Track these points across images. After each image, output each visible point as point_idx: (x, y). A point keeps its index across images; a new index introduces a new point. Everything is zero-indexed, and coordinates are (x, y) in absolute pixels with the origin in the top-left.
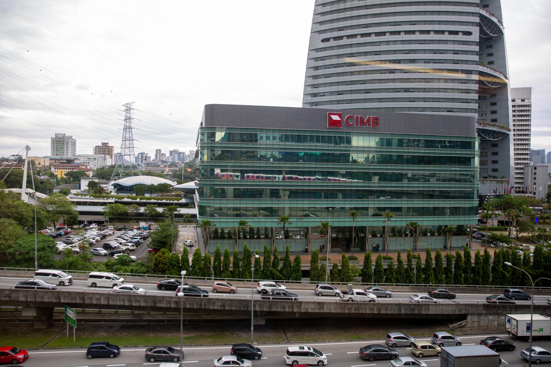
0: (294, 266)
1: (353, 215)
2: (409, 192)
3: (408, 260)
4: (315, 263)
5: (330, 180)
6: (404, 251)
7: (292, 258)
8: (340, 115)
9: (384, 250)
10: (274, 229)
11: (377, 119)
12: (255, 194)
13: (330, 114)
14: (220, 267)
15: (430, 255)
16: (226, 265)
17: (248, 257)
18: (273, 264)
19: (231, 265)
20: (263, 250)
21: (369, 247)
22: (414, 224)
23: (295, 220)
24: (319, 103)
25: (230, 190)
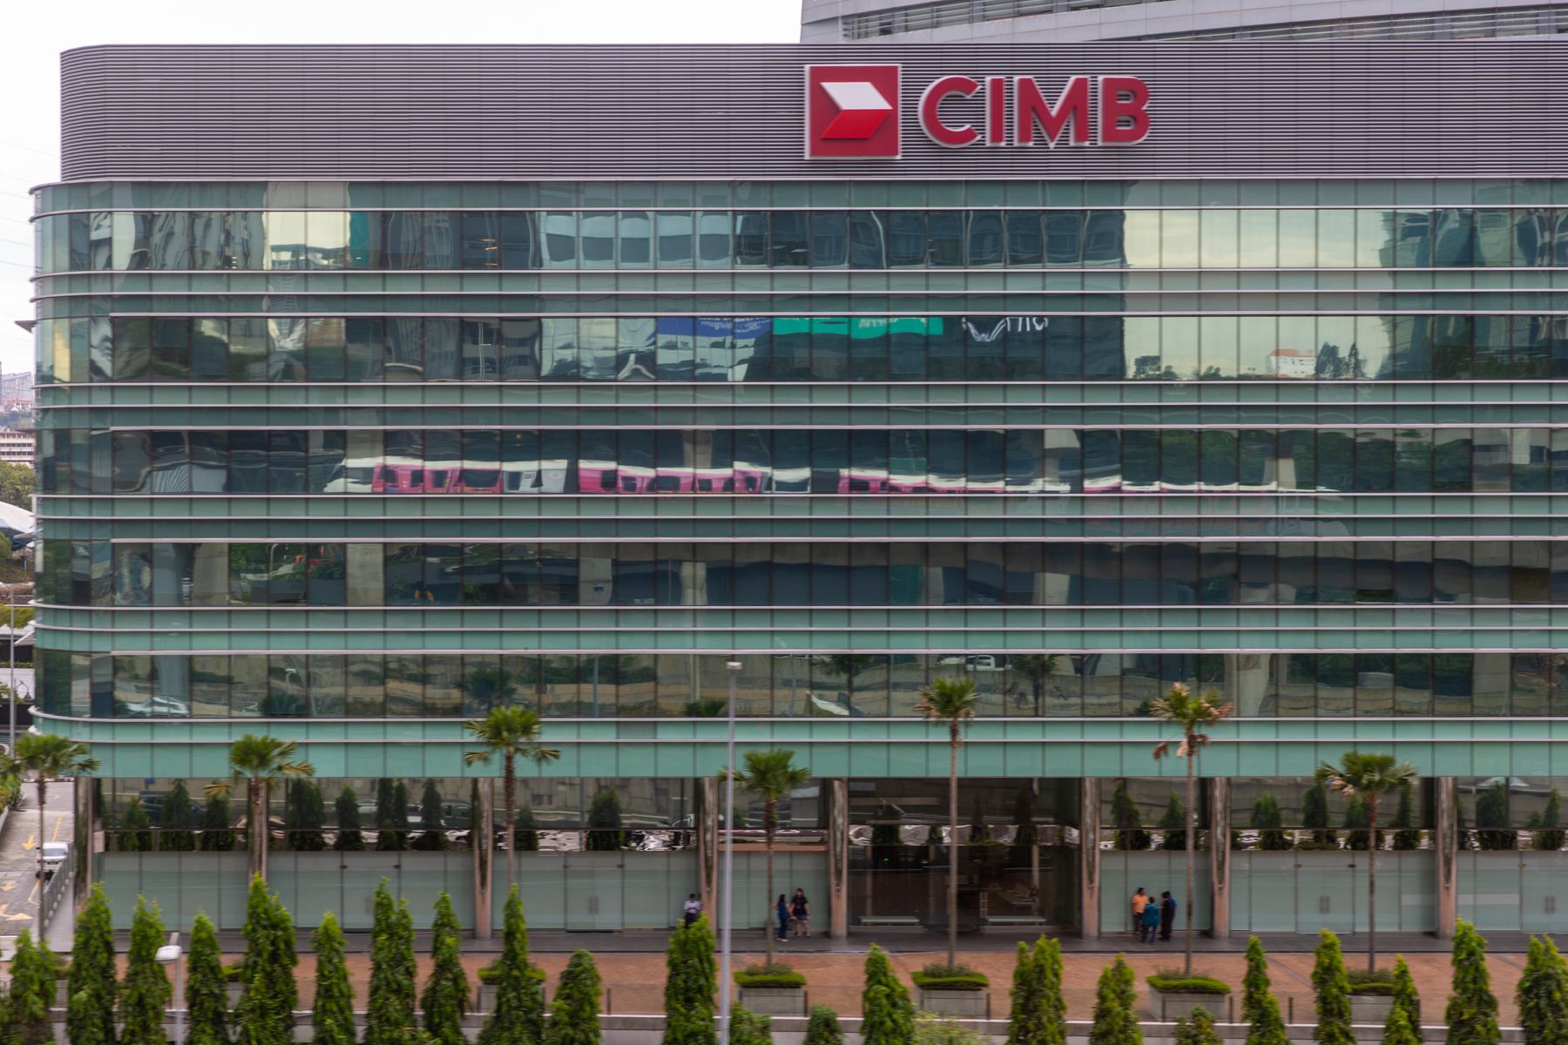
0: (554, 1024)
1: (949, 704)
2: (1401, 556)
3: (1323, 1000)
4: (689, 1002)
5: (858, 485)
6: (1293, 943)
7: (549, 969)
8: (884, 81)
9: (1208, 934)
10: (1445, 799)
11: (1138, 91)
12: (544, 578)
13: (820, 75)
14: (108, 1017)
15: (1479, 976)
16: (141, 1003)
17: (274, 958)
18: (430, 1002)
19: (179, 1008)
20: (366, 920)
21: (1104, 910)
22: (1369, 766)
23: (609, 736)
24: (899, 19)
25: (364, 557)
